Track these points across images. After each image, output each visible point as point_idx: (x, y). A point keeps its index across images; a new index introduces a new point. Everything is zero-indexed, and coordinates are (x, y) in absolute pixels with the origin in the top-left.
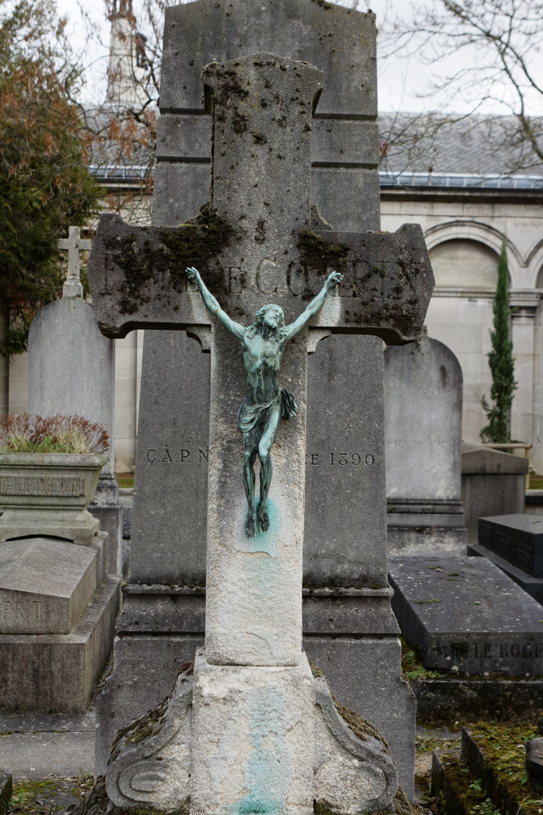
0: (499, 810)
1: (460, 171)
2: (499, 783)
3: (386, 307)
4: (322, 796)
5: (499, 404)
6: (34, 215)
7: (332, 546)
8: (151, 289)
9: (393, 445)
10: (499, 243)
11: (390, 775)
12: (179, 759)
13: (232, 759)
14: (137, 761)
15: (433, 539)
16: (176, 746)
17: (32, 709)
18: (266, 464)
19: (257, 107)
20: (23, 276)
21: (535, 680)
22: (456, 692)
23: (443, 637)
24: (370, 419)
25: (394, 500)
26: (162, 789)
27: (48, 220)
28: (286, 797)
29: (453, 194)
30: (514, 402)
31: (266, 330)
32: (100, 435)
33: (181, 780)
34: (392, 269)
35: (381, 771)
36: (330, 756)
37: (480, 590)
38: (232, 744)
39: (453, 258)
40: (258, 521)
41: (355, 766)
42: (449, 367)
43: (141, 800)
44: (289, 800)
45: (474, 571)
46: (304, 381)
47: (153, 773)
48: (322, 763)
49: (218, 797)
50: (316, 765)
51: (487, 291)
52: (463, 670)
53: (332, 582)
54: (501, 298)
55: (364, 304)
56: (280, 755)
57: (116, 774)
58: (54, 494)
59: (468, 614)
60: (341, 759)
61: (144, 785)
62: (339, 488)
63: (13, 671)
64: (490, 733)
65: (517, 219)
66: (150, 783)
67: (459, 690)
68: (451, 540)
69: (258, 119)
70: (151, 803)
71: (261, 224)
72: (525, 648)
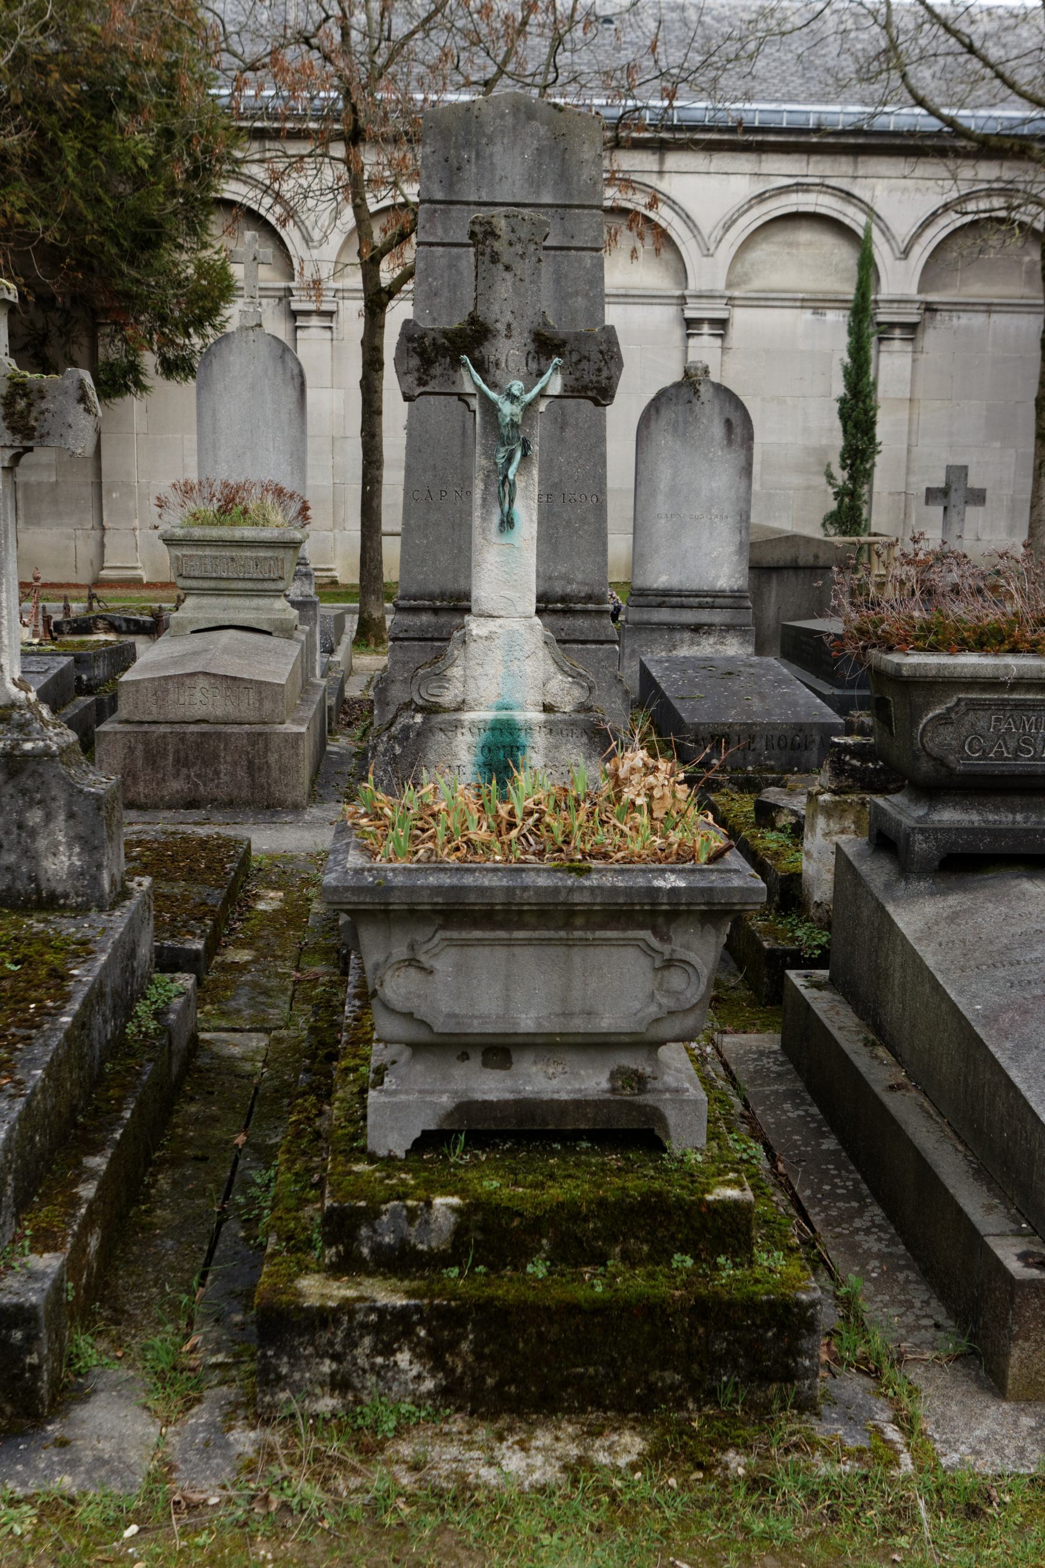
1: (806, 101)
3: (591, 381)
5: (851, 477)
6: (139, 180)
7: (563, 570)
8: (437, 370)
9: (663, 521)
10: (862, 219)
15: (712, 640)
17: (247, 804)
18: (513, 485)
19: (506, 246)
20: (122, 274)
24: (595, 465)
25: (663, 591)
27: (161, 186)
29: (792, 139)
30: (877, 473)
31: (512, 398)
32: (299, 506)
34: (595, 356)
39: (790, 245)
40: (507, 523)
42: (736, 420)
45: (752, 671)
46: (537, 431)
48: (548, 680)
51: (841, 297)
53: (563, 599)
54: (861, 310)
55: (577, 379)
58: (247, 576)
61: (435, 691)
62: (569, 522)
65: (893, 181)
68: (735, 641)
69: (507, 255)
71: (509, 326)
72: (793, 740)
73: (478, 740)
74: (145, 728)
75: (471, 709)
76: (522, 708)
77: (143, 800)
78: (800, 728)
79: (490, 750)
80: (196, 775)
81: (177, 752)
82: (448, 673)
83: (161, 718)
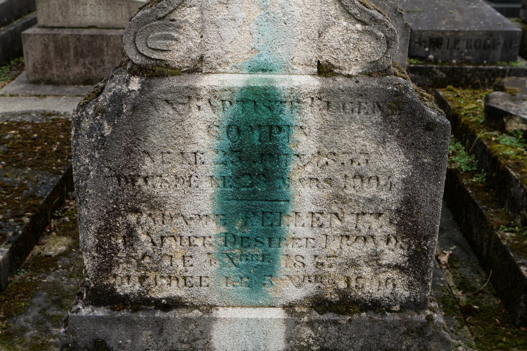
0: (460, 142)
2: (462, 122)
4: (325, 58)
11: (391, 39)
12: (191, 21)
13: (241, 20)
14: (151, 22)
16: (188, 9)
21: (490, 65)
22: (430, 73)
23: (424, 34)
26: (176, 48)
28: (292, 57)
33: (194, 40)
35: (383, 35)
36: (334, 20)
37: (454, 4)
38: (241, 5)
41: (357, 30)
43: (157, 57)
44: (295, 60)
47: (167, 33)
48: (326, 27)
49: (229, 56)
50: (321, 29)
52: (437, 58)
56: (286, 17)
57: (132, 33)
59: (444, 19)
60: (345, 24)
61: (159, 44)
63: (108, 55)
64: (456, 93)
66: (165, 42)
67: (433, 72)
70: (167, 61)
72: (485, 42)
73: (221, 116)
74: (55, 31)
75: (213, 70)
76: (288, 70)
77: (56, 79)
78: (490, 34)
79: (239, 131)
80: (90, 63)
81: (76, 48)
82: (178, 16)
83: (66, 25)
